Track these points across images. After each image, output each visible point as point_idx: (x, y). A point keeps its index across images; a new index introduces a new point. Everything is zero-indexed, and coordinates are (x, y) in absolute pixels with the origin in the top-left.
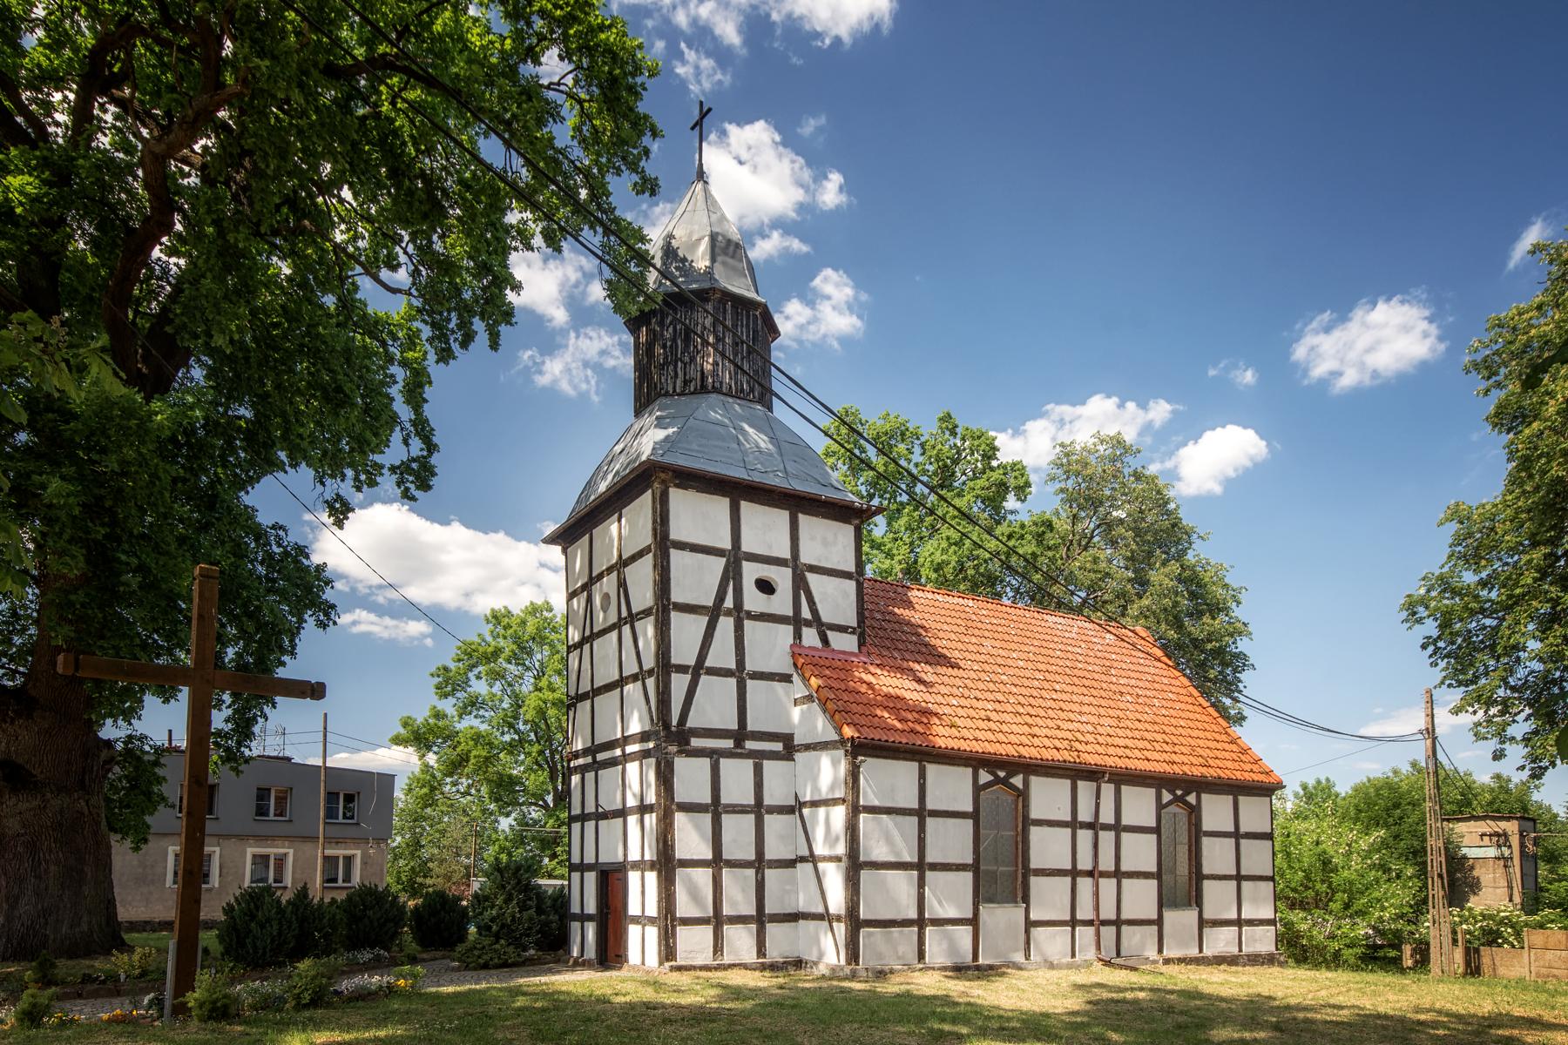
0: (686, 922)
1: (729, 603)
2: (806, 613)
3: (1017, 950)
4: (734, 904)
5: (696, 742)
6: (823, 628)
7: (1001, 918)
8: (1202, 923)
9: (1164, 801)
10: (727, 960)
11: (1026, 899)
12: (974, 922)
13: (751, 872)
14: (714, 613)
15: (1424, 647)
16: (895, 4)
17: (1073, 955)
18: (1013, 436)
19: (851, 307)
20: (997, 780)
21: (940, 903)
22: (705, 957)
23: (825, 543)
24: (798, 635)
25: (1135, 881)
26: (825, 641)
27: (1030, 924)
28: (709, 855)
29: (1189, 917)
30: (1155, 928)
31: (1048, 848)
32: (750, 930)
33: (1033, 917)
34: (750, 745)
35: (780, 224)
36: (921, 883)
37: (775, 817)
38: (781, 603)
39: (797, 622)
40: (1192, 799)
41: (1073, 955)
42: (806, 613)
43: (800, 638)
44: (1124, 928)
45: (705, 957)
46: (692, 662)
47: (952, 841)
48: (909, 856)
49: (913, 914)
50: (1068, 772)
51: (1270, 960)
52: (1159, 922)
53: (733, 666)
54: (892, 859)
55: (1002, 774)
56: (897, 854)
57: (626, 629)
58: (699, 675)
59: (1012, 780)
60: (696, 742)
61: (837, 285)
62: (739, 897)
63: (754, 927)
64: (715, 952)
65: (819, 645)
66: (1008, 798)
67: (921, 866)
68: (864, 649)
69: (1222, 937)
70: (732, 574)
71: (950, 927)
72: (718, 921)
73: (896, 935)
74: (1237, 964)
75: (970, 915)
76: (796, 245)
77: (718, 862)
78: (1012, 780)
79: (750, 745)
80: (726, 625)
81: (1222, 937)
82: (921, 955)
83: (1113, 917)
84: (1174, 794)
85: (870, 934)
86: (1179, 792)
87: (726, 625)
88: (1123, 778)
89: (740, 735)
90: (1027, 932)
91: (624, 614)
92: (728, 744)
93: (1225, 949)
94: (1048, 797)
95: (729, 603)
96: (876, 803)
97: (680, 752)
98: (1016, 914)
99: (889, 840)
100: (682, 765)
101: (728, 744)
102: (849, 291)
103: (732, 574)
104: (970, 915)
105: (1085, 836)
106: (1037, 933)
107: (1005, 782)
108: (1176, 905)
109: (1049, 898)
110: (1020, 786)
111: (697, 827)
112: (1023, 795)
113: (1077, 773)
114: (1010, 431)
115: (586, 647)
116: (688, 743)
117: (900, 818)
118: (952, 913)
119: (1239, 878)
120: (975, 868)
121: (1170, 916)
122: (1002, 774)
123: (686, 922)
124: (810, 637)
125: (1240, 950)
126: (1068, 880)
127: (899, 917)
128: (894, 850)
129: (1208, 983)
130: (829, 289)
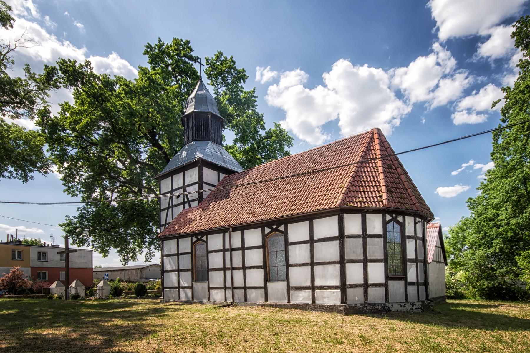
7: (200, 286)
9: (193, 241)
11: (208, 280)
17: (226, 300)
20: (273, 230)
21: (184, 283)
25: (252, 270)
27: (210, 288)
29: (281, 286)
30: (263, 290)
31: (216, 260)
33: (211, 286)
37: (379, 258)
40: (400, 219)
41: (226, 300)
44: (248, 290)
47: (186, 262)
48: (175, 268)
49: (176, 285)
50: (260, 225)
54: (171, 269)
55: (199, 237)
57: (170, 210)
59: (279, 229)
66: (397, 228)
67: (178, 271)
73: (172, 291)
74: (307, 310)
75: (191, 285)
78: (279, 229)
81: (301, 295)
83: (338, 292)
84: (392, 217)
86: (274, 227)
88: (243, 228)
90: (209, 291)
91: (171, 205)
93: (303, 302)
98: (205, 284)
104: (191, 285)
107: (276, 230)
110: (401, 221)
113: (223, 230)
117: (172, 257)
118: (186, 285)
120: (192, 270)
122: (199, 237)
125: (314, 301)
126: (222, 272)
127: (174, 286)
128: (172, 268)
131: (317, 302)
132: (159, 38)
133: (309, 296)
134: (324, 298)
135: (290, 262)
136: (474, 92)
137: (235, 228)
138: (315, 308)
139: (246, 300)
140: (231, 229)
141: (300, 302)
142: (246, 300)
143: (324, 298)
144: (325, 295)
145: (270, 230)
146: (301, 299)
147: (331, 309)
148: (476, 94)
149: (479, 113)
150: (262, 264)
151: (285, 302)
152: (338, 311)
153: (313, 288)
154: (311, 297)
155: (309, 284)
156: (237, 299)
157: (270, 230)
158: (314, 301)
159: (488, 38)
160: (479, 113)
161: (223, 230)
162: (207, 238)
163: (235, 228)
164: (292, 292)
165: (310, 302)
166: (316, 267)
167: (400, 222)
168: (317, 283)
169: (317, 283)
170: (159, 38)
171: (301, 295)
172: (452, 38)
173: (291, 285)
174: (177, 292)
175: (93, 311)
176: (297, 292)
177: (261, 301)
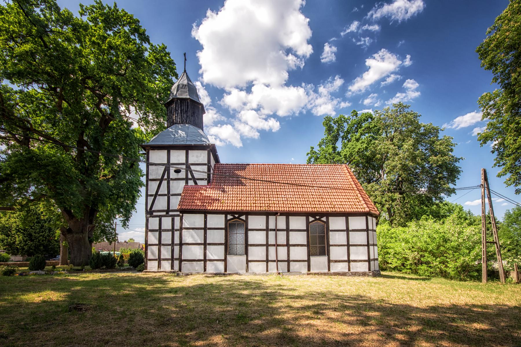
0: (150, 260)
1: (166, 177)
2: (190, 176)
3: (242, 269)
4: (164, 255)
5: (155, 214)
6: (195, 180)
8: (329, 261)
10: (162, 270)
12: (225, 260)
13: (170, 247)
14: (161, 180)
15: (493, 152)
16: (304, 3)
18: (477, 112)
19: (417, 90)
21: (212, 254)
22: (156, 269)
23: (197, 157)
24: (187, 183)
26: (196, 183)
28: (157, 243)
32: (169, 263)
34: (171, 213)
35: (392, 73)
36: (205, 249)
38: (182, 175)
39: (187, 179)
42: (190, 176)
43: (188, 184)
45: (156, 269)
46: (154, 193)
51: (364, 274)
52: (309, 261)
53: (166, 193)
55: (237, 216)
56: (195, 241)
58: (156, 197)
59: (241, 218)
60: (155, 214)
61: (412, 84)
62: (166, 254)
63: (170, 261)
64: (158, 268)
65: (194, 184)
68: (209, 184)
69: (340, 266)
70: (167, 170)
71: (216, 262)
72: (159, 260)
74: (346, 275)
76: (399, 76)
77: (160, 244)
78: (241, 218)
79: (171, 213)
80: (165, 183)
82: (205, 270)
85: (185, 264)
87: (165, 183)
88: (288, 214)
89: (168, 211)
90: (247, 263)
92: (164, 213)
93: (341, 270)
94: (337, 223)
95: (166, 177)
96: (188, 226)
97: (150, 217)
98: (324, 259)
99: (192, 237)
100: (151, 219)
101: (164, 213)
102: (417, 85)
103: (167, 170)
105: (272, 234)
106: (250, 264)
108: (315, 255)
109: (258, 253)
111: (154, 236)
112: (327, 223)
113: (267, 214)
114: (476, 111)
115: (490, 191)
116: (153, 214)
119: (348, 245)
121: (312, 259)
123: (150, 260)
124: (191, 183)
125: (349, 270)
129: (440, 283)
130: (409, 85)
131: (352, 270)
132: (115, 3)
133: (346, 267)
134: (357, 267)
135: (250, 242)
136: (219, 125)
137: (282, 214)
138: (352, 274)
139: (289, 271)
140: (279, 214)
141: (339, 270)
142: (289, 271)
143: (357, 267)
144: (358, 266)
145: (314, 219)
146: (339, 268)
147: (364, 274)
148: (220, 127)
149: (221, 140)
150: (306, 243)
151: (326, 271)
152: (368, 275)
153: (349, 261)
154: (347, 267)
155: (346, 259)
156: (281, 269)
157: (314, 219)
158: (349, 270)
159: (229, 93)
160: (221, 140)
161: (267, 214)
162: (247, 218)
163: (282, 214)
164: (331, 264)
165: (347, 271)
166: (351, 248)
167: (309, 220)
168: (352, 258)
169: (352, 258)
170: (115, 3)
171: (340, 266)
172: (210, 83)
173: (331, 259)
174: (203, 265)
175: (135, 285)
176: (336, 264)
177: (305, 271)
